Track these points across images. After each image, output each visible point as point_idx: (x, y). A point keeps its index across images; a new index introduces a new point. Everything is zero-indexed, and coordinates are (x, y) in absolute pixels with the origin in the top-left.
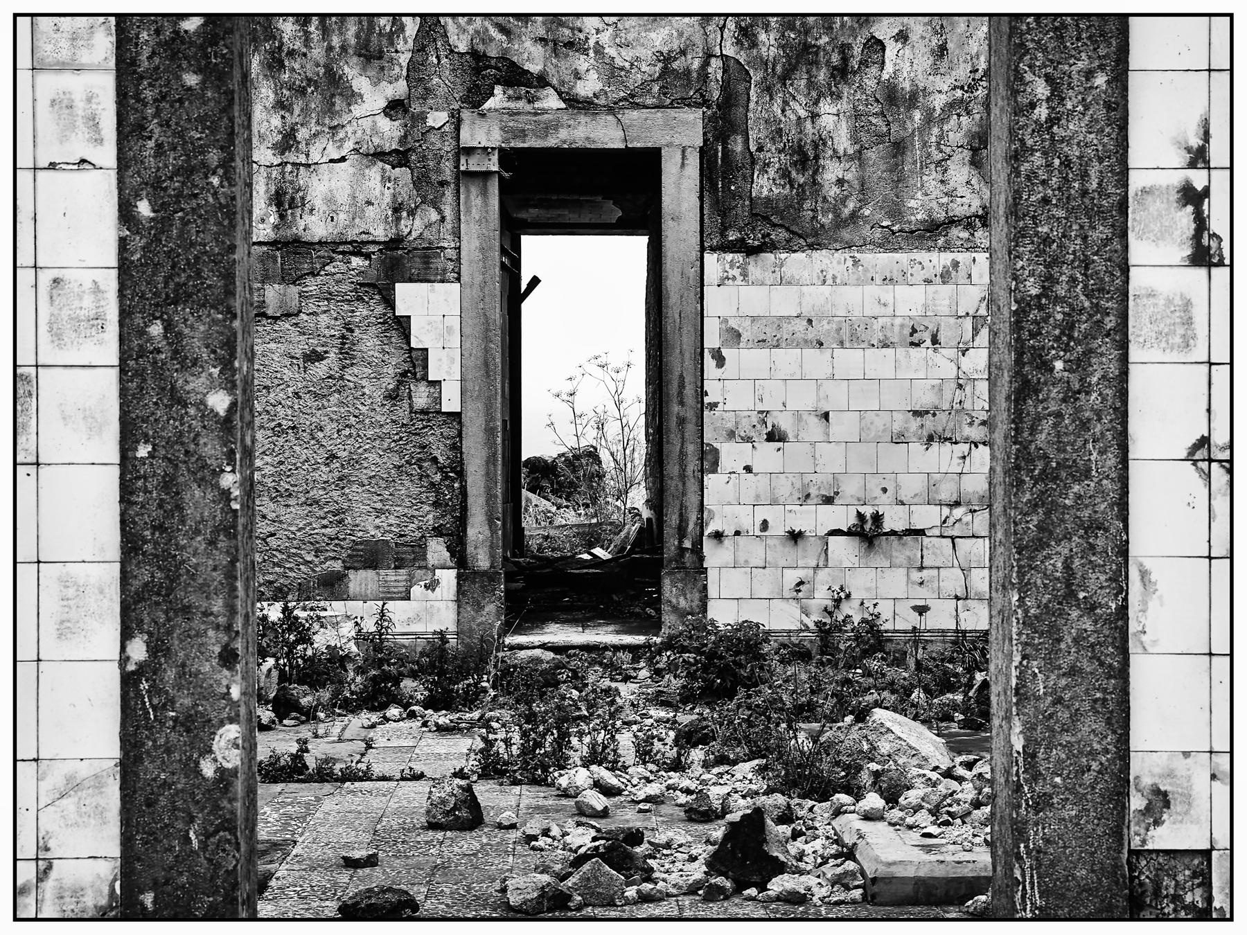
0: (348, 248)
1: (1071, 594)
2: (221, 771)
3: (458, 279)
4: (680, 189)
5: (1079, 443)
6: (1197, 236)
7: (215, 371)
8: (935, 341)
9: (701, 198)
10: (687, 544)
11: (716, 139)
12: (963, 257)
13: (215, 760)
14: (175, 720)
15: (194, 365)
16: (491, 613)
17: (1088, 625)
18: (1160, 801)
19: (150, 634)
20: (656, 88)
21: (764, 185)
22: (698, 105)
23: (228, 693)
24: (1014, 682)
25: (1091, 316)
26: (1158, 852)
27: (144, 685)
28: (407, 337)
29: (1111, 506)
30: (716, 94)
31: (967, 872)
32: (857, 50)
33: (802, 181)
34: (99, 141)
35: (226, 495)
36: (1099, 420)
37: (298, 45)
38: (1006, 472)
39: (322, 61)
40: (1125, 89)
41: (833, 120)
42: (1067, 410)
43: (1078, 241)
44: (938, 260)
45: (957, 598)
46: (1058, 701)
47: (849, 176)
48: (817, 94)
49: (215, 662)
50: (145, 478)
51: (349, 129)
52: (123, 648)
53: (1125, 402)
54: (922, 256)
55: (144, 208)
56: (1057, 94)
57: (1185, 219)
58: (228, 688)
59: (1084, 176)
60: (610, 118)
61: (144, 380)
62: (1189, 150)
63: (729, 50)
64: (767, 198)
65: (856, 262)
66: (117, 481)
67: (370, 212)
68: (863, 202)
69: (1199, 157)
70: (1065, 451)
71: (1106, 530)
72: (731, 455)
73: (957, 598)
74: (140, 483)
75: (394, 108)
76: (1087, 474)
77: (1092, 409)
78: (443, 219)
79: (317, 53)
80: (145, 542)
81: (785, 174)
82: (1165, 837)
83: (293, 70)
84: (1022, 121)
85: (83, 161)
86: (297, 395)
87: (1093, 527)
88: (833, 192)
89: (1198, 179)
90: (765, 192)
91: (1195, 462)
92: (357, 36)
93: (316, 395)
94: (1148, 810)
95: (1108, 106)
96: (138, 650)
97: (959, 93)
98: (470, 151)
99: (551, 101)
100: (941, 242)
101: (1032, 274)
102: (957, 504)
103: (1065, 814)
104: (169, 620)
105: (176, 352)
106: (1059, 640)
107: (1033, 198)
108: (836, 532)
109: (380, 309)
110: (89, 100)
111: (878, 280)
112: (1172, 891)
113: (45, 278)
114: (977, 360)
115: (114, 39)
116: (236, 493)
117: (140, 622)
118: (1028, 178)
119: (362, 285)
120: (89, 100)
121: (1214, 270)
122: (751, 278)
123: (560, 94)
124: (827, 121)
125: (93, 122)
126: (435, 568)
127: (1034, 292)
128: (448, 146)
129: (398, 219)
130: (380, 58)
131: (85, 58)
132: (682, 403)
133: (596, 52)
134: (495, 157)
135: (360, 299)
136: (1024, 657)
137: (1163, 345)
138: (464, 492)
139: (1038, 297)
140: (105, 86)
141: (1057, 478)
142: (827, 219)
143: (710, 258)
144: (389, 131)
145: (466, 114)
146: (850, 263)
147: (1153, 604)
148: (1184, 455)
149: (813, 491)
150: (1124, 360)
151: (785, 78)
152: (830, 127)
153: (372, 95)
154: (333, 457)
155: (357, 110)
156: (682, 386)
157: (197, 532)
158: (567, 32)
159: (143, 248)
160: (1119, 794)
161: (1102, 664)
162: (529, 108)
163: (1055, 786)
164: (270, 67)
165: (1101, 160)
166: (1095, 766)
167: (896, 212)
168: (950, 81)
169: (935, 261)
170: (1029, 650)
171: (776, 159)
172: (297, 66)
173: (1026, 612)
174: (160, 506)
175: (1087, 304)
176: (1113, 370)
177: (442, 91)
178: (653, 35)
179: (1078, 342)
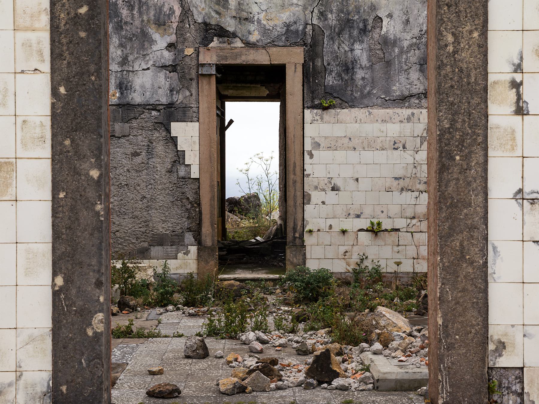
0: (151, 107)
1: (463, 257)
2: (95, 333)
3: (198, 121)
4: (294, 82)
5: (466, 192)
8: (404, 147)
9: (303, 85)
10: (297, 235)
11: (310, 60)
12: (415, 111)
13: (93, 328)
14: (76, 311)
15: (84, 158)
16: (213, 264)
17: (470, 270)
18: (502, 346)
19: (65, 274)
20: (284, 38)
21: (330, 80)
22: (302, 46)
23: (99, 300)
24: (438, 294)
27: (62, 296)
28: (176, 146)
29: (480, 219)
30: (310, 41)
32: (370, 21)
33: (347, 78)
34: (43, 61)
35: (98, 214)
36: (475, 181)
37: (129, 19)
38: (435, 204)
39: (139, 26)
41: (360, 52)
42: (461, 177)
43: (466, 104)
44: (406, 112)
45: (414, 259)
46: (458, 303)
47: (367, 76)
48: (353, 41)
50: (63, 207)
51: (151, 56)
52: (53, 280)
55: (62, 90)
56: (457, 41)
57: (512, 95)
58: (99, 297)
59: (469, 76)
60: (264, 51)
62: (514, 65)
63: (315, 22)
64: (331, 85)
65: (370, 114)
67: (160, 91)
68: (373, 88)
69: (518, 68)
70: (460, 195)
71: (478, 229)
72: (316, 197)
74: (60, 209)
75: (171, 46)
76: (470, 205)
77: (472, 177)
78: (191, 95)
79: (137, 23)
82: (503, 362)
83: (126, 30)
84: (442, 52)
87: (472, 228)
88: (360, 83)
89: (518, 77)
90: (331, 83)
92: (154, 16)
93: (137, 171)
94: (496, 350)
95: (479, 46)
96: (59, 281)
97: (415, 40)
98: (203, 65)
99: (238, 44)
101: (446, 118)
102: (414, 218)
105: (76, 152)
106: (458, 277)
107: (446, 86)
108: (361, 230)
109: (164, 134)
110: (39, 43)
111: (380, 121)
112: (506, 385)
113: (19, 120)
114: (422, 156)
115: (49, 17)
118: (444, 77)
119: (156, 123)
120: (39, 43)
121: (525, 117)
122: (324, 120)
124: (357, 52)
126: (188, 245)
127: (447, 126)
128: (194, 63)
129: (172, 95)
130: (164, 25)
131: (37, 25)
132: (295, 174)
134: (214, 68)
135: (155, 129)
136: (443, 284)
138: (200, 213)
139: (449, 128)
140: (45, 37)
141: (457, 206)
142: (357, 95)
143: (307, 112)
144: (168, 57)
145: (201, 49)
146: (367, 113)
147: (498, 261)
149: (352, 212)
150: (486, 156)
151: (339, 34)
152: (359, 55)
153: (160, 41)
154: (145, 197)
155: (155, 48)
156: (295, 167)
157: (85, 230)
158: (245, 14)
159: (62, 107)
160: (484, 343)
161: (476, 287)
163: (456, 339)
165: (476, 69)
167: (387, 91)
168: (411, 35)
170: (445, 281)
172: (128, 29)
173: (443, 264)
174: (69, 219)
175: (470, 131)
176: (481, 160)
178: (282, 15)
179: (466, 148)
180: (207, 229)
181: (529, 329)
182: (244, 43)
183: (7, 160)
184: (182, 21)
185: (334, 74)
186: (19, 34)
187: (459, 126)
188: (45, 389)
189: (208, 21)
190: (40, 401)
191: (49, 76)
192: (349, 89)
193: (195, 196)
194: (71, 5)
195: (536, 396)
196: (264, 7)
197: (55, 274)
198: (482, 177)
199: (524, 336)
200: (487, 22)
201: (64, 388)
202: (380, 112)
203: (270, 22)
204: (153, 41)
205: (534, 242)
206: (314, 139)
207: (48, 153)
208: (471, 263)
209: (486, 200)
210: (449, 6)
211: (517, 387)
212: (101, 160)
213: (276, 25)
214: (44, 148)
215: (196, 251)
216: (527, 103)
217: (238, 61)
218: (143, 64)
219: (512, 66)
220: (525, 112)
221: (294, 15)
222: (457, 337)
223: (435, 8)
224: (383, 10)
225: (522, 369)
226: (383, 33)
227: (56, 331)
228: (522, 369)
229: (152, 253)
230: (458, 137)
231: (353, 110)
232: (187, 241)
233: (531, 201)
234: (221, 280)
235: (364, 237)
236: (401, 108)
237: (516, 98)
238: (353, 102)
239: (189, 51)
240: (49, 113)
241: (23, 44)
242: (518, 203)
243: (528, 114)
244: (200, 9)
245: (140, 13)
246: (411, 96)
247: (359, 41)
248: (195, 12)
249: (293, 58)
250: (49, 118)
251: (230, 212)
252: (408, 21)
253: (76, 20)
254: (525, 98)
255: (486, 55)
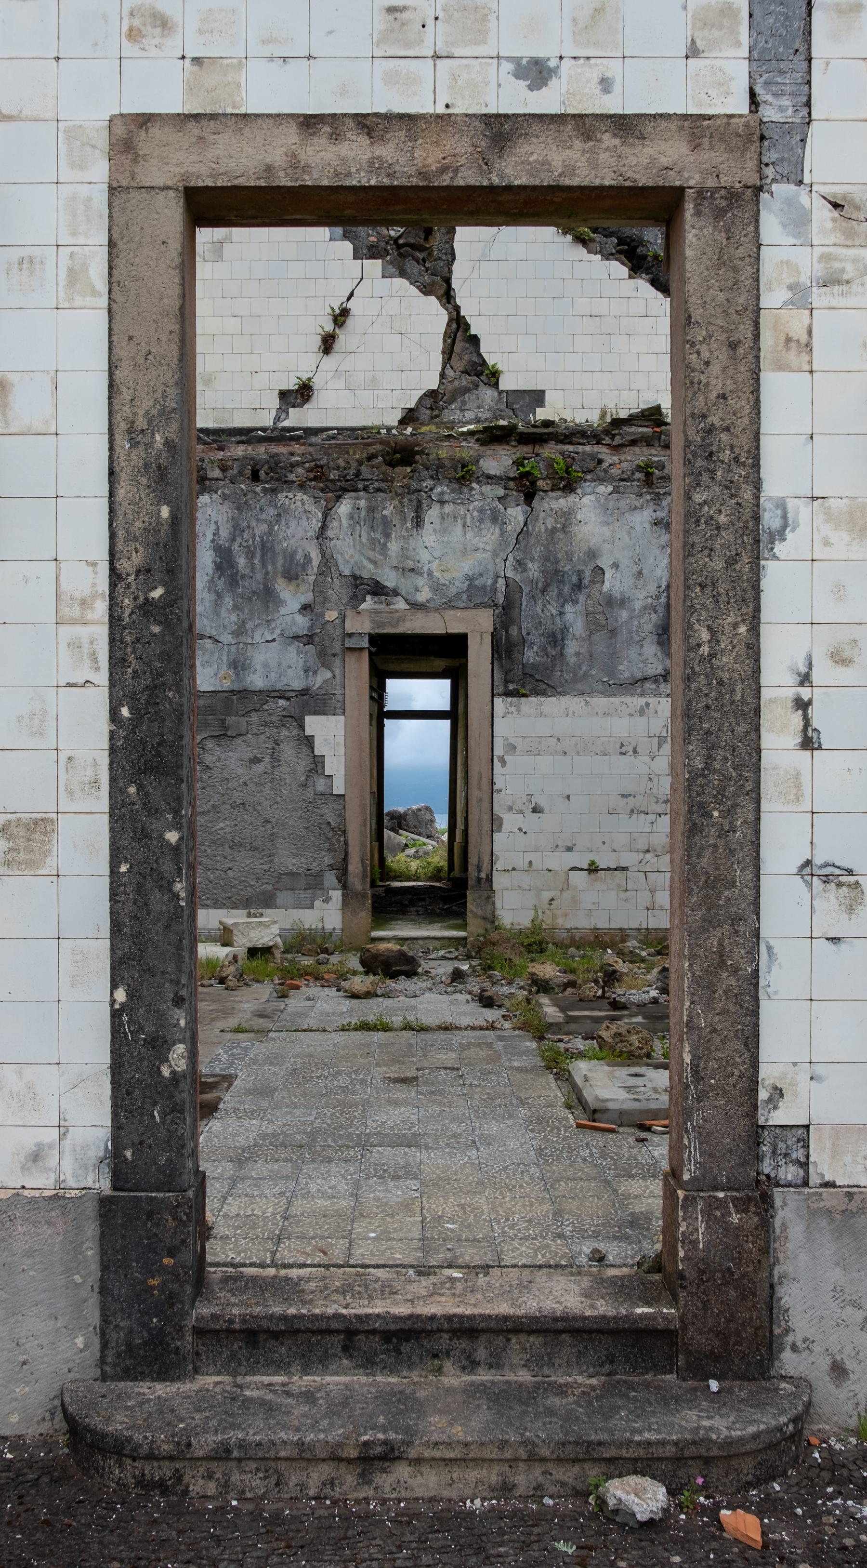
0: (277, 694)
1: (722, 964)
2: (174, 1073)
3: (344, 714)
4: (479, 657)
5: (729, 864)
6: (805, 730)
7: (170, 817)
8: (635, 751)
9: (492, 663)
10: (483, 875)
11: (502, 628)
12: (652, 700)
13: (170, 1066)
14: (144, 1040)
15: (156, 812)
16: (364, 915)
17: (733, 981)
18: (778, 1092)
19: (129, 985)
20: (465, 597)
21: (530, 656)
22: (490, 607)
23: (178, 1024)
24: (685, 1018)
25: (736, 782)
26: (776, 1126)
27: (125, 1018)
28: (312, 748)
29: (749, 905)
30: (501, 600)
31: (653, 1106)
32: (588, 573)
33: (554, 653)
34: (98, 669)
35: (177, 896)
36: (742, 849)
37: (247, 571)
38: (682, 882)
39: (261, 581)
40: (758, 635)
41: (574, 617)
42: (721, 842)
43: (729, 733)
44: (638, 702)
45: (648, 909)
46: (715, 1030)
47: (583, 651)
48: (563, 600)
49: (170, 1003)
50: (125, 886)
51: (278, 622)
52: (112, 994)
53: (758, 839)
54: (628, 699)
55: (125, 712)
56: (714, 638)
57: (797, 719)
58: (178, 1020)
59: (733, 691)
60: (437, 615)
61: (124, 822)
62: (799, 674)
63: (510, 574)
64: (533, 664)
65: (587, 703)
66: (108, 887)
67: (291, 672)
68: (591, 667)
69: (805, 679)
70: (719, 869)
71: (746, 920)
72: (510, 821)
73: (648, 909)
74: (122, 889)
75: (306, 608)
76: (733, 885)
77: (737, 843)
78: (334, 677)
79: (259, 576)
80: (125, 926)
81: (544, 649)
82: (779, 1117)
83: (244, 586)
84: (692, 655)
85: (88, 682)
86: (245, 784)
87: (737, 919)
88: (572, 660)
89: (805, 693)
90: (531, 660)
91: (802, 876)
92: (283, 566)
93: (257, 784)
94: (770, 1100)
95: (748, 646)
96: (121, 995)
97: (650, 600)
98: (350, 635)
99: (401, 605)
100: (639, 691)
101: (698, 754)
102: (648, 851)
103: (716, 1103)
104: (140, 976)
105: (144, 804)
106: (714, 992)
107: (699, 705)
108: (573, 869)
109: (295, 732)
110: (92, 643)
111: (600, 714)
112: (784, 1151)
113: (63, 756)
114: (662, 764)
115: (107, 603)
116: (183, 895)
117: (123, 979)
118: (696, 692)
119: (285, 716)
120: (92, 643)
121: (815, 752)
122: (522, 713)
123: (406, 600)
124: (569, 617)
125: (94, 656)
126: (328, 889)
127: (700, 766)
128: (338, 632)
129: (307, 677)
130: (297, 579)
131: (90, 616)
132: (480, 789)
133: (429, 574)
134: (366, 639)
135: (284, 725)
136: (692, 1003)
137: (783, 800)
138: (346, 843)
139: (703, 769)
140: (102, 632)
141: (714, 887)
142: (568, 676)
143: (498, 701)
144: (302, 623)
145: (349, 613)
146: (583, 703)
147: (775, 968)
148: (795, 871)
149: (560, 844)
150: (758, 810)
151: (544, 591)
152: (572, 620)
153: (292, 598)
154: (268, 821)
155: (283, 611)
156: (480, 778)
157: (159, 920)
158: (411, 563)
159: (124, 738)
160: (752, 1090)
161: (742, 1007)
162: (387, 609)
163: (711, 1086)
164: (231, 585)
165: (743, 680)
166: (736, 1072)
167: (611, 671)
168: (644, 593)
169: (635, 703)
170: (695, 998)
171: (536, 638)
172: (246, 584)
173: (693, 974)
174: (135, 903)
175: (734, 774)
176: (751, 817)
177: (334, 598)
178: (463, 564)
179: (728, 799)
180: (355, 866)
181: (819, 1069)
182: (409, 604)
183: (44, 816)
184: (321, 573)
185: (535, 648)
186: (62, 629)
187: (717, 765)
188: (101, 1154)
189: (358, 573)
190: (94, 1170)
191: (106, 690)
192: (558, 668)
193: (339, 820)
194: (140, 587)
195: (826, 1167)
196: (437, 554)
197: (114, 986)
198: (752, 842)
199: (812, 1078)
200: (759, 611)
201: (128, 1154)
202: (601, 702)
203: (445, 575)
204: (280, 601)
205: (827, 939)
206: (507, 739)
207: (104, 805)
208: (736, 971)
209: (758, 877)
210: (703, 586)
211: (800, 1154)
212: (181, 817)
213: (454, 579)
214: (98, 798)
215: (340, 898)
216: (819, 732)
217: (401, 629)
218: (266, 633)
219: (796, 676)
220: (816, 746)
221: (480, 563)
222: (712, 1081)
223: (681, 588)
224: (605, 557)
225: (807, 1127)
226: (605, 589)
227: (116, 1068)
228: (807, 1127)
229: (278, 900)
230: (716, 782)
231: (563, 698)
232: (327, 884)
233: (824, 878)
234: (374, 940)
235: (580, 879)
236: (632, 696)
237: (802, 724)
238: (563, 686)
239: (331, 615)
240: (106, 746)
241: (69, 645)
242: (805, 881)
243: (820, 748)
244: (347, 557)
245: (264, 564)
246: (645, 679)
247: (572, 601)
248: (340, 561)
249: (478, 626)
250: (107, 753)
251: (392, 829)
252: (640, 573)
253: (146, 608)
254: (815, 724)
255: (757, 660)
